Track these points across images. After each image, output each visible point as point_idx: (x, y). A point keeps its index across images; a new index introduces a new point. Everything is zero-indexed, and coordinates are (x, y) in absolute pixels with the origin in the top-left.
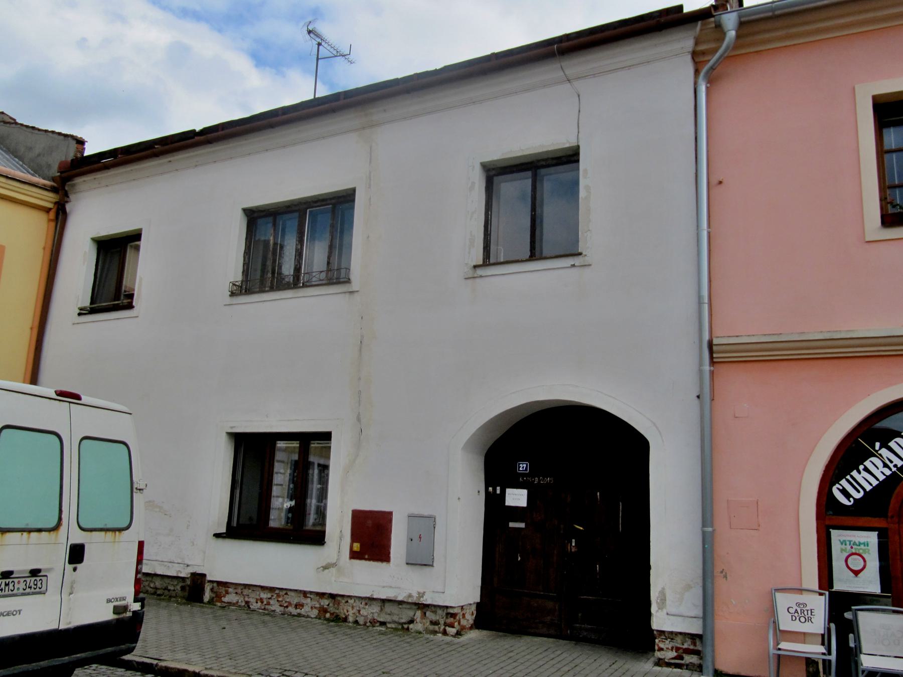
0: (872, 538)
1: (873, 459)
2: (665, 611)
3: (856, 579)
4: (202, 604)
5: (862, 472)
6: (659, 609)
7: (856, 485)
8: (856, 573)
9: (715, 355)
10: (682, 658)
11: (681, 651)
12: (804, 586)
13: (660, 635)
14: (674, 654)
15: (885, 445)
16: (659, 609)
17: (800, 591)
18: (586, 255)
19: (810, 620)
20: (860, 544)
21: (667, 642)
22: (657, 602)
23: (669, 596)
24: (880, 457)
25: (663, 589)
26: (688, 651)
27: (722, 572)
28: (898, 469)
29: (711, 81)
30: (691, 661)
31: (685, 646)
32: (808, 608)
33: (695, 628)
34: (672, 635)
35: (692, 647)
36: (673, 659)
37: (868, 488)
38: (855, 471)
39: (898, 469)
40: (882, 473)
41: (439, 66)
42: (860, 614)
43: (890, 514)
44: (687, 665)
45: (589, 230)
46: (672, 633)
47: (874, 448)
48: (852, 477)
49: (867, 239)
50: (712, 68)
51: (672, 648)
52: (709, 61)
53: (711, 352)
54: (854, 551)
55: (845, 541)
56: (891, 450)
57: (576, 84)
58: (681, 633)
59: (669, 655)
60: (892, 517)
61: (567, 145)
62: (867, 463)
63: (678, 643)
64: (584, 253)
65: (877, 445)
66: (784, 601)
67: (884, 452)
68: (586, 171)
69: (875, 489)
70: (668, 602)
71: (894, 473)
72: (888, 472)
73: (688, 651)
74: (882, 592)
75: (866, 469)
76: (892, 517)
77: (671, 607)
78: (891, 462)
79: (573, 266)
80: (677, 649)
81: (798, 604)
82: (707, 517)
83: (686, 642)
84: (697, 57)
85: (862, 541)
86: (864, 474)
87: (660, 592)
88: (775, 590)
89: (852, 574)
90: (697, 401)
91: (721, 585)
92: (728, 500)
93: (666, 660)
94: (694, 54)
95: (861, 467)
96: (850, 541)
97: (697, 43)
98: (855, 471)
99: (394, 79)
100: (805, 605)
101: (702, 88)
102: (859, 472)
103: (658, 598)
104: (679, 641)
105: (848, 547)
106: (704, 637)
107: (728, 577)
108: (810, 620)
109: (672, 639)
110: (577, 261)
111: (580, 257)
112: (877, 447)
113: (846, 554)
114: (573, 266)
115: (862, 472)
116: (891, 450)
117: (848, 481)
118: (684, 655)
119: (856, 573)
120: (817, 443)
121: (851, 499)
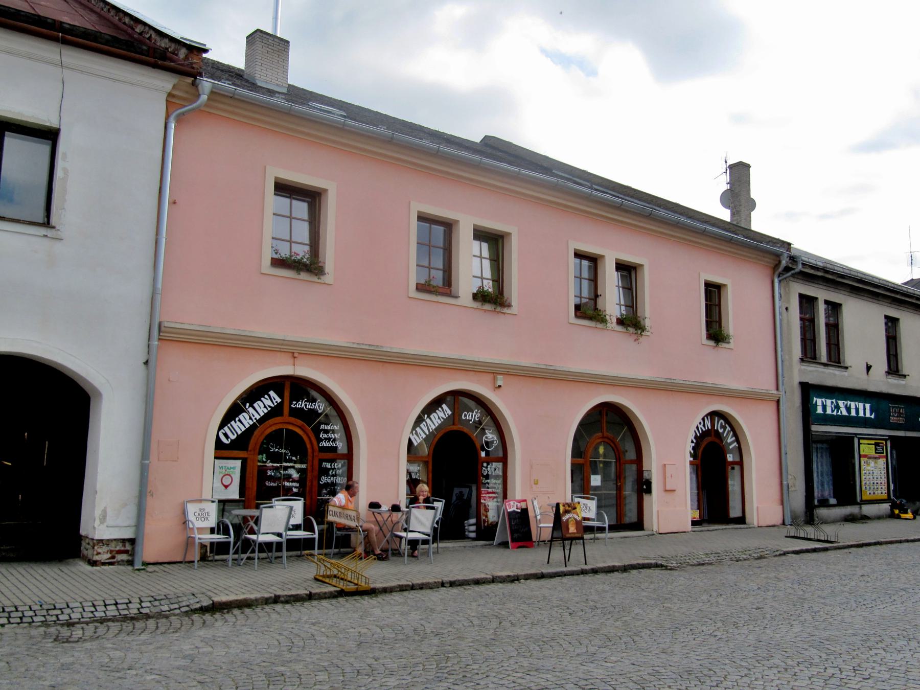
0: (238, 463)
1: (244, 414)
2: (105, 524)
3: (226, 490)
4: (206, 562)
5: (237, 422)
6: (101, 523)
7: (233, 430)
8: (226, 487)
9: (161, 334)
10: (113, 557)
11: (114, 552)
12: (203, 498)
13: (98, 543)
14: (109, 555)
15: (251, 406)
16: (101, 523)
17: (201, 501)
18: (59, 230)
19: (207, 519)
20: (231, 468)
21: (104, 547)
22: (100, 519)
23: (110, 513)
24: (248, 413)
25: (105, 508)
26: (119, 552)
27: (150, 492)
28: (257, 421)
29: (179, 120)
30: (122, 558)
31: (118, 548)
32: (206, 511)
33: (128, 534)
34: (107, 542)
35: (123, 549)
36: (108, 559)
37: (239, 432)
38: (233, 421)
39: (257, 421)
40: (248, 423)
41: (583, 169)
42: (413, 509)
43: (249, 449)
44: (118, 562)
45: (64, 209)
46: (108, 540)
47: (245, 407)
48: (231, 425)
49: (262, 272)
50: (183, 114)
51: (108, 551)
52: (185, 106)
53: (160, 331)
54: (227, 473)
55: (222, 467)
56: (430, 419)
57: (65, 71)
58: (115, 540)
59: (105, 557)
60: (251, 451)
61: (48, 124)
62: (241, 417)
63: (112, 547)
64: (58, 228)
65: (248, 405)
66: (192, 509)
67: (251, 410)
68: (64, 154)
69: (243, 433)
70: (108, 518)
71: (254, 423)
72: (251, 423)
73: (119, 552)
74: (240, 498)
75: (240, 420)
76: (251, 451)
77: (110, 521)
78: (254, 416)
79: (45, 236)
80: (111, 552)
81: (200, 510)
82: (145, 453)
83: (118, 545)
84: (171, 100)
85: (232, 466)
86: (238, 423)
87: (103, 510)
88: (187, 502)
89: (224, 488)
90: (143, 366)
91: (150, 503)
92: (159, 441)
93: (102, 561)
94: (170, 95)
95: (237, 419)
96: (225, 467)
97: (174, 87)
98: (233, 421)
99: (385, 115)
100: (204, 509)
101: (172, 125)
102: (236, 422)
103: (100, 515)
104: (113, 546)
105: (224, 470)
106: (137, 540)
107: (154, 495)
108: (207, 519)
109: (108, 545)
110: (49, 232)
111: (54, 230)
112: (247, 407)
113: (222, 475)
114: (45, 236)
115: (237, 422)
116: (430, 419)
117: (229, 428)
118: (116, 555)
119: (226, 487)
120: (220, 403)
121: (229, 440)
